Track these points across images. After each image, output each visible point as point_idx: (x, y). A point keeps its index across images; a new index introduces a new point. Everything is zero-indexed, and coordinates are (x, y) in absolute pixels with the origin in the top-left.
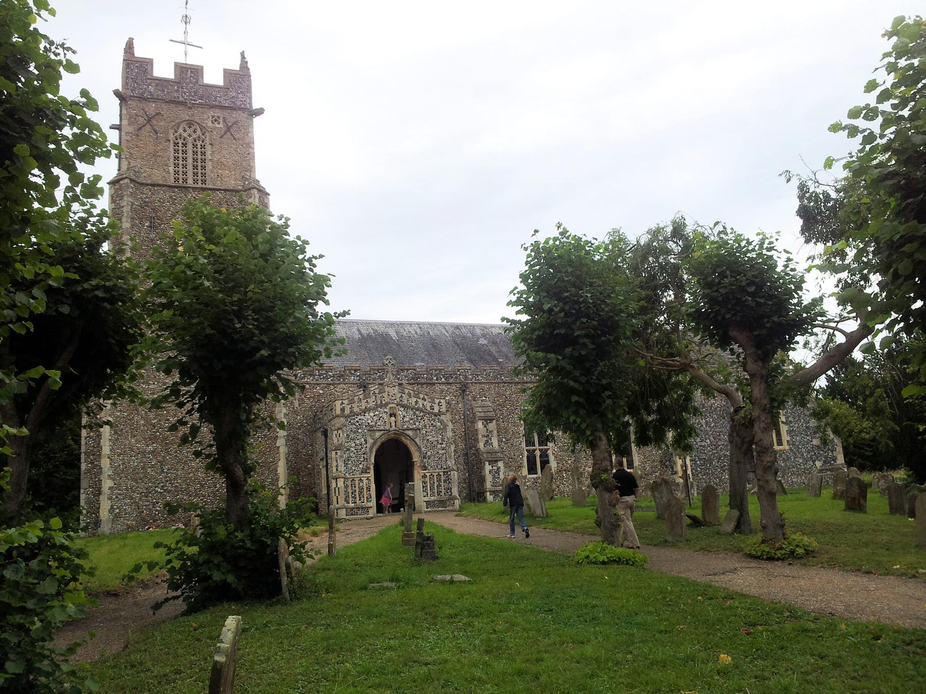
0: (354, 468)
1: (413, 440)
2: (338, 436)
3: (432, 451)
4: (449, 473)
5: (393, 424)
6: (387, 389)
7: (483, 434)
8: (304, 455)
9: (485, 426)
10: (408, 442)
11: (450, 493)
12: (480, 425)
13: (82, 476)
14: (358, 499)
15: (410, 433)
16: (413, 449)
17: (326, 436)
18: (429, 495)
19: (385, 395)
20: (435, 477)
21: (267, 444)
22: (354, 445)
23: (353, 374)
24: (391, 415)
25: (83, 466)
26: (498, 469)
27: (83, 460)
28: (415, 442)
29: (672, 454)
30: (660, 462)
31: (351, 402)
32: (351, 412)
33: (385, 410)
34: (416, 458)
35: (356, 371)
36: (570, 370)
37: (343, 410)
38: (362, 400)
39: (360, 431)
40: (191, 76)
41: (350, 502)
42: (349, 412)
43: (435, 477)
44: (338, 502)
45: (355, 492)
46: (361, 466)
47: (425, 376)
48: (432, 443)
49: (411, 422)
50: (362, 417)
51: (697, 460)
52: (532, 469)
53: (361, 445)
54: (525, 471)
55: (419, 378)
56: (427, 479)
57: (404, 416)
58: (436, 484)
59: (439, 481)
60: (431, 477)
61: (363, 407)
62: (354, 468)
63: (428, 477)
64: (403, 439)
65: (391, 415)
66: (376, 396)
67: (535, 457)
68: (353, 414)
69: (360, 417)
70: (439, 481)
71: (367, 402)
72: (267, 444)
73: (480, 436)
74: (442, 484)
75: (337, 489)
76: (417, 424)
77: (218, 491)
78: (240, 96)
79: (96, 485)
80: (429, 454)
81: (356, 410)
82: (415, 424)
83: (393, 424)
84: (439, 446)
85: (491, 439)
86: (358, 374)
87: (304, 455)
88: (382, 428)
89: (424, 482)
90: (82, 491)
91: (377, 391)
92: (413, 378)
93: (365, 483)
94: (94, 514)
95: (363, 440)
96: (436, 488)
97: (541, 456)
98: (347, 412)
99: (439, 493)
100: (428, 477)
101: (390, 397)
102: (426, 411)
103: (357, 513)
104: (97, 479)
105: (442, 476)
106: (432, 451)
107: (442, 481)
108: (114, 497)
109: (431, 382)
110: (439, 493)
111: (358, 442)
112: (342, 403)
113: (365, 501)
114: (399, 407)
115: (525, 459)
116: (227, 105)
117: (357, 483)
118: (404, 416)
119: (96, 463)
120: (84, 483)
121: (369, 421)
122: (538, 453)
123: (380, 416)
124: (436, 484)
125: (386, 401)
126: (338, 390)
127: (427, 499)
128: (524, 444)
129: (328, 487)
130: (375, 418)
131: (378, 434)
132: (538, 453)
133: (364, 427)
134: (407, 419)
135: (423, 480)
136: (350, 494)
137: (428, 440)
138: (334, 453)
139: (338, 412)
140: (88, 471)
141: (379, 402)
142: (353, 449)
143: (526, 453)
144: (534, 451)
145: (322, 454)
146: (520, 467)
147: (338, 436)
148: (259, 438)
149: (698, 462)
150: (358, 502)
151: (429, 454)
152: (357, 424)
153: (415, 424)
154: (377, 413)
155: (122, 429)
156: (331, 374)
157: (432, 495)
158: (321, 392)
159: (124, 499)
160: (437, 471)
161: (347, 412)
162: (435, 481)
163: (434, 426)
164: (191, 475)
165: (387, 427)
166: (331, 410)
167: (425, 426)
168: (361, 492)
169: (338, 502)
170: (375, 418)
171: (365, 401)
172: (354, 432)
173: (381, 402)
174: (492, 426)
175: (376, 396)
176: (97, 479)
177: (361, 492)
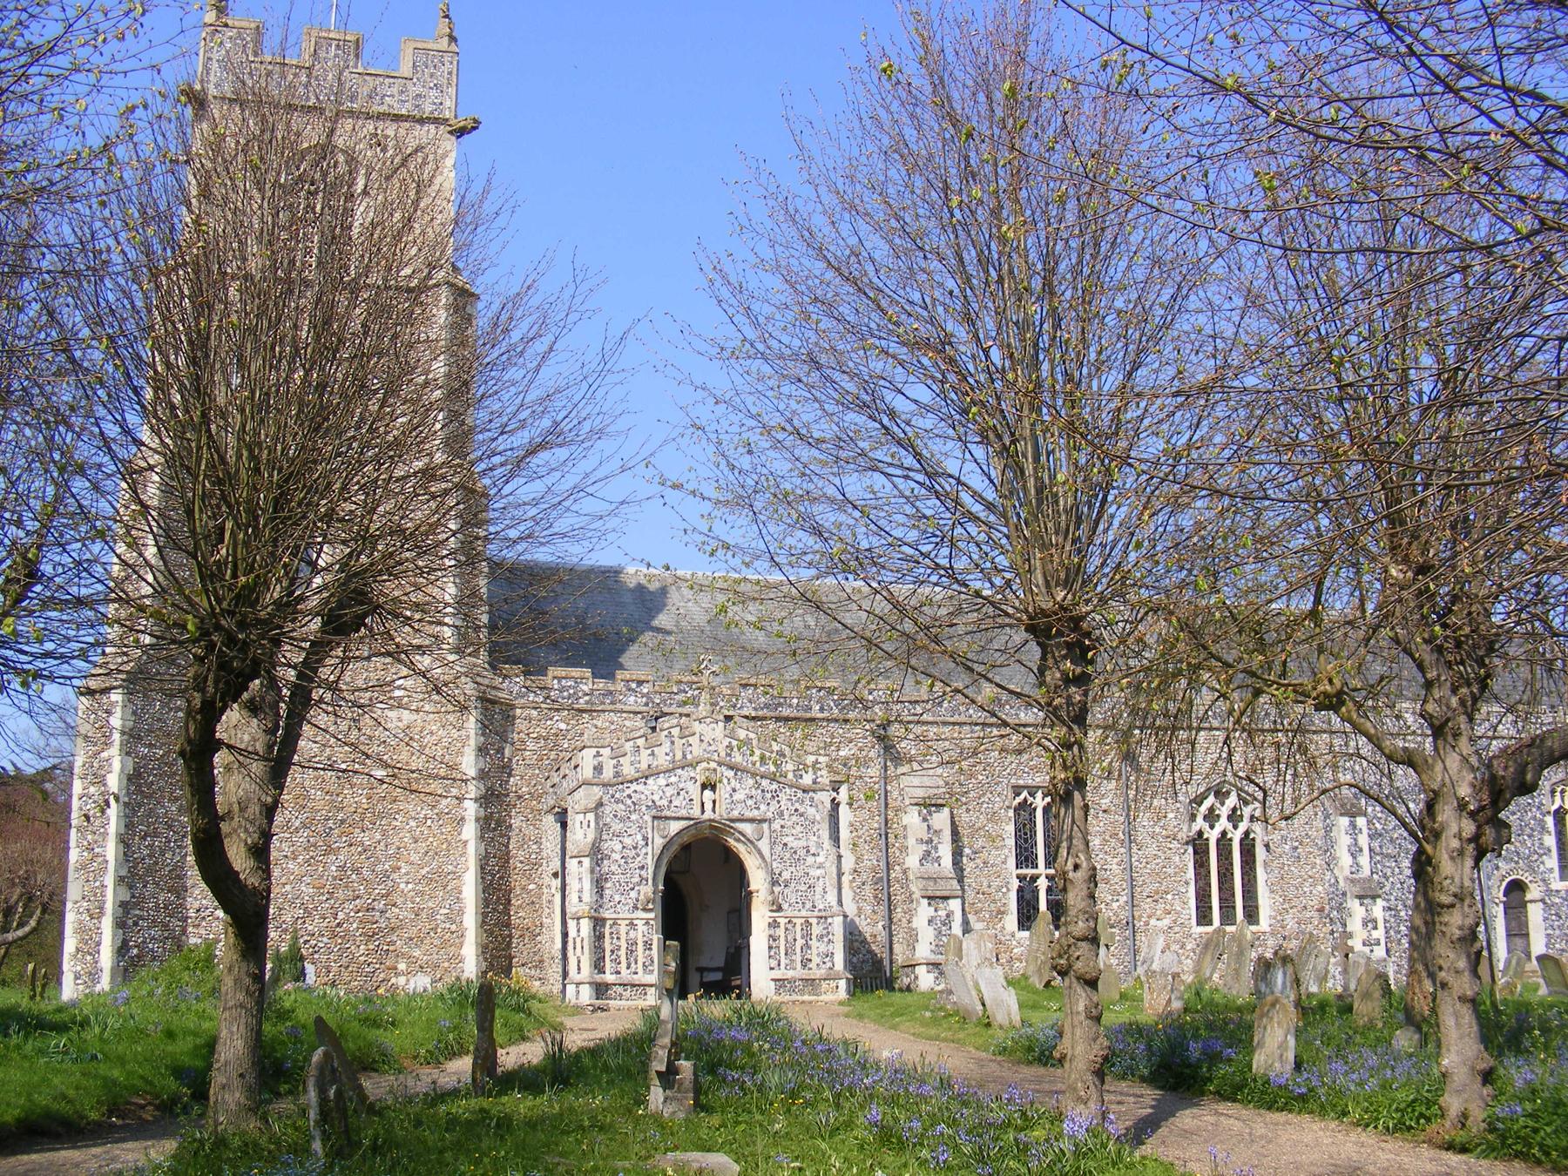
0: (617, 898)
1: (751, 842)
2: (585, 825)
3: (793, 869)
4: (830, 920)
5: (708, 806)
6: (697, 727)
7: (920, 836)
8: (521, 862)
9: (925, 820)
10: (741, 849)
11: (829, 965)
12: (912, 818)
13: (71, 875)
14: (624, 965)
15: (747, 828)
16: (751, 863)
17: (564, 825)
18: (783, 966)
19: (694, 740)
20: (798, 928)
21: (442, 833)
22: (618, 847)
23: (633, 690)
24: (704, 787)
25: (74, 855)
26: (948, 916)
27: (73, 843)
28: (755, 847)
29: (1344, 894)
30: (1318, 910)
31: (618, 756)
32: (617, 774)
33: (693, 775)
34: (757, 880)
35: (640, 683)
36: (191, 1046)
37: (598, 769)
38: (642, 750)
39: (634, 817)
40: (336, 56)
41: (608, 971)
42: (611, 774)
43: (798, 928)
44: (579, 969)
45: (618, 950)
46: (633, 894)
47: (795, 701)
48: (795, 852)
49: (750, 802)
50: (640, 788)
51: (1400, 907)
52: (1027, 916)
53: (635, 848)
54: (1011, 921)
55: (780, 705)
56: (781, 932)
57: (734, 790)
58: (800, 942)
59: (807, 936)
60: (789, 926)
61: (644, 766)
62: (617, 898)
63: (782, 926)
64: (731, 841)
65: (704, 787)
66: (673, 743)
67: (1036, 891)
68: (620, 781)
69: (634, 786)
70: (807, 936)
71: (653, 754)
72: (442, 833)
73: (911, 842)
74: (814, 943)
75: (578, 941)
76: (763, 807)
77: (338, 925)
78: (433, 93)
79: (95, 895)
80: (786, 875)
81: (628, 770)
82: (758, 808)
83: (708, 806)
84: (810, 860)
85: (936, 848)
86: (645, 691)
87: (521, 862)
88: (683, 813)
89: (773, 938)
90: (69, 905)
91: (675, 732)
92: (767, 706)
93: (640, 931)
94: (90, 954)
95: (639, 837)
96: (798, 950)
97: (1049, 890)
98: (608, 773)
99: (805, 963)
100: (782, 926)
101: (705, 745)
102: (782, 780)
103: (621, 995)
104: (97, 884)
105: (814, 925)
106: (793, 869)
107: (814, 937)
108: (130, 922)
109: (808, 715)
110: (805, 963)
111: (628, 841)
112: (598, 754)
113: (640, 970)
114: (724, 768)
115: (1013, 896)
116: (404, 112)
117: (623, 929)
118: (734, 790)
119: (96, 850)
120: (74, 891)
121: (656, 798)
122: (1042, 884)
123: (681, 786)
124: (800, 942)
125: (695, 753)
126: (599, 724)
127: (777, 974)
128: (1012, 862)
129: (565, 935)
130: (670, 791)
131: (675, 827)
132: (1042, 884)
133: (644, 808)
134: (739, 796)
135: (772, 932)
136: (608, 953)
137: (785, 845)
138: (575, 861)
139: (587, 772)
140: (83, 867)
141: (679, 756)
142: (616, 856)
143: (1015, 884)
144: (1034, 878)
145: (556, 864)
146: (1001, 913)
147: (585, 825)
148: (426, 819)
149: (1403, 914)
150: (624, 972)
151: (786, 875)
152: (629, 802)
153: (758, 808)
154: (673, 779)
155: (152, 782)
156: (585, 688)
157: (788, 967)
158: (563, 726)
159: (149, 928)
160: (804, 913)
161: (608, 773)
162: (798, 936)
163: (801, 815)
164: (288, 888)
165: (696, 812)
166: (576, 767)
167: (781, 814)
168: (631, 951)
169: (579, 969)
170: (670, 791)
171: (649, 751)
172: (622, 820)
173: (684, 756)
174: (941, 819)
175: (673, 743)
176: (97, 884)
177: (631, 951)
